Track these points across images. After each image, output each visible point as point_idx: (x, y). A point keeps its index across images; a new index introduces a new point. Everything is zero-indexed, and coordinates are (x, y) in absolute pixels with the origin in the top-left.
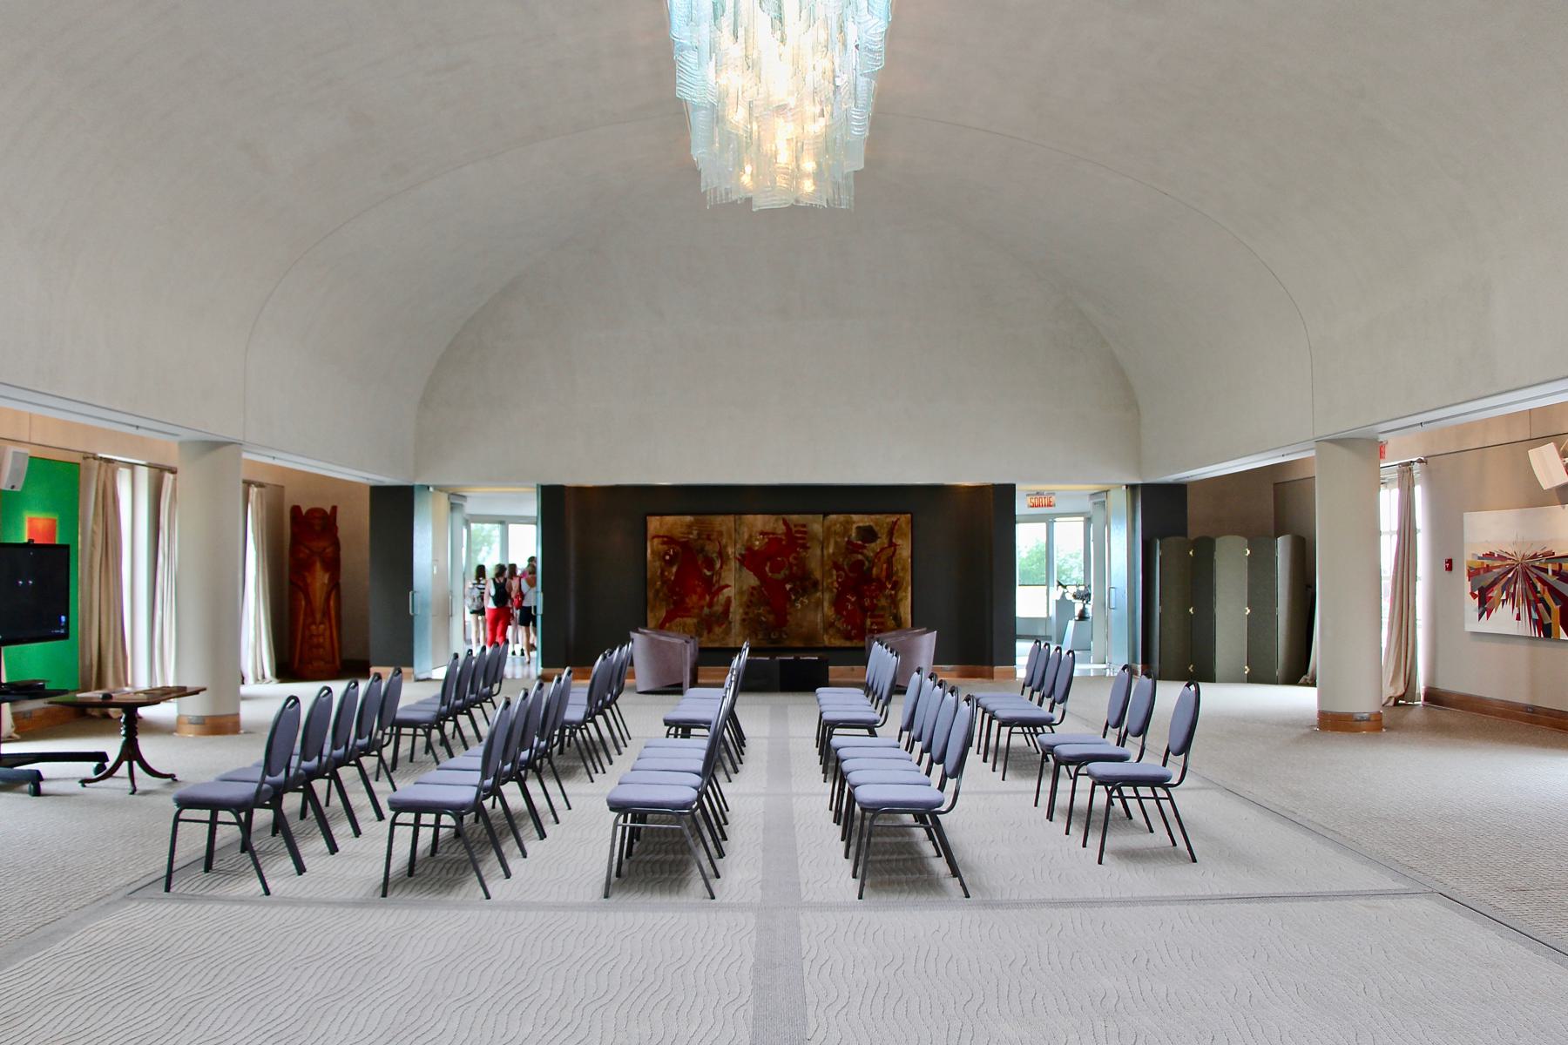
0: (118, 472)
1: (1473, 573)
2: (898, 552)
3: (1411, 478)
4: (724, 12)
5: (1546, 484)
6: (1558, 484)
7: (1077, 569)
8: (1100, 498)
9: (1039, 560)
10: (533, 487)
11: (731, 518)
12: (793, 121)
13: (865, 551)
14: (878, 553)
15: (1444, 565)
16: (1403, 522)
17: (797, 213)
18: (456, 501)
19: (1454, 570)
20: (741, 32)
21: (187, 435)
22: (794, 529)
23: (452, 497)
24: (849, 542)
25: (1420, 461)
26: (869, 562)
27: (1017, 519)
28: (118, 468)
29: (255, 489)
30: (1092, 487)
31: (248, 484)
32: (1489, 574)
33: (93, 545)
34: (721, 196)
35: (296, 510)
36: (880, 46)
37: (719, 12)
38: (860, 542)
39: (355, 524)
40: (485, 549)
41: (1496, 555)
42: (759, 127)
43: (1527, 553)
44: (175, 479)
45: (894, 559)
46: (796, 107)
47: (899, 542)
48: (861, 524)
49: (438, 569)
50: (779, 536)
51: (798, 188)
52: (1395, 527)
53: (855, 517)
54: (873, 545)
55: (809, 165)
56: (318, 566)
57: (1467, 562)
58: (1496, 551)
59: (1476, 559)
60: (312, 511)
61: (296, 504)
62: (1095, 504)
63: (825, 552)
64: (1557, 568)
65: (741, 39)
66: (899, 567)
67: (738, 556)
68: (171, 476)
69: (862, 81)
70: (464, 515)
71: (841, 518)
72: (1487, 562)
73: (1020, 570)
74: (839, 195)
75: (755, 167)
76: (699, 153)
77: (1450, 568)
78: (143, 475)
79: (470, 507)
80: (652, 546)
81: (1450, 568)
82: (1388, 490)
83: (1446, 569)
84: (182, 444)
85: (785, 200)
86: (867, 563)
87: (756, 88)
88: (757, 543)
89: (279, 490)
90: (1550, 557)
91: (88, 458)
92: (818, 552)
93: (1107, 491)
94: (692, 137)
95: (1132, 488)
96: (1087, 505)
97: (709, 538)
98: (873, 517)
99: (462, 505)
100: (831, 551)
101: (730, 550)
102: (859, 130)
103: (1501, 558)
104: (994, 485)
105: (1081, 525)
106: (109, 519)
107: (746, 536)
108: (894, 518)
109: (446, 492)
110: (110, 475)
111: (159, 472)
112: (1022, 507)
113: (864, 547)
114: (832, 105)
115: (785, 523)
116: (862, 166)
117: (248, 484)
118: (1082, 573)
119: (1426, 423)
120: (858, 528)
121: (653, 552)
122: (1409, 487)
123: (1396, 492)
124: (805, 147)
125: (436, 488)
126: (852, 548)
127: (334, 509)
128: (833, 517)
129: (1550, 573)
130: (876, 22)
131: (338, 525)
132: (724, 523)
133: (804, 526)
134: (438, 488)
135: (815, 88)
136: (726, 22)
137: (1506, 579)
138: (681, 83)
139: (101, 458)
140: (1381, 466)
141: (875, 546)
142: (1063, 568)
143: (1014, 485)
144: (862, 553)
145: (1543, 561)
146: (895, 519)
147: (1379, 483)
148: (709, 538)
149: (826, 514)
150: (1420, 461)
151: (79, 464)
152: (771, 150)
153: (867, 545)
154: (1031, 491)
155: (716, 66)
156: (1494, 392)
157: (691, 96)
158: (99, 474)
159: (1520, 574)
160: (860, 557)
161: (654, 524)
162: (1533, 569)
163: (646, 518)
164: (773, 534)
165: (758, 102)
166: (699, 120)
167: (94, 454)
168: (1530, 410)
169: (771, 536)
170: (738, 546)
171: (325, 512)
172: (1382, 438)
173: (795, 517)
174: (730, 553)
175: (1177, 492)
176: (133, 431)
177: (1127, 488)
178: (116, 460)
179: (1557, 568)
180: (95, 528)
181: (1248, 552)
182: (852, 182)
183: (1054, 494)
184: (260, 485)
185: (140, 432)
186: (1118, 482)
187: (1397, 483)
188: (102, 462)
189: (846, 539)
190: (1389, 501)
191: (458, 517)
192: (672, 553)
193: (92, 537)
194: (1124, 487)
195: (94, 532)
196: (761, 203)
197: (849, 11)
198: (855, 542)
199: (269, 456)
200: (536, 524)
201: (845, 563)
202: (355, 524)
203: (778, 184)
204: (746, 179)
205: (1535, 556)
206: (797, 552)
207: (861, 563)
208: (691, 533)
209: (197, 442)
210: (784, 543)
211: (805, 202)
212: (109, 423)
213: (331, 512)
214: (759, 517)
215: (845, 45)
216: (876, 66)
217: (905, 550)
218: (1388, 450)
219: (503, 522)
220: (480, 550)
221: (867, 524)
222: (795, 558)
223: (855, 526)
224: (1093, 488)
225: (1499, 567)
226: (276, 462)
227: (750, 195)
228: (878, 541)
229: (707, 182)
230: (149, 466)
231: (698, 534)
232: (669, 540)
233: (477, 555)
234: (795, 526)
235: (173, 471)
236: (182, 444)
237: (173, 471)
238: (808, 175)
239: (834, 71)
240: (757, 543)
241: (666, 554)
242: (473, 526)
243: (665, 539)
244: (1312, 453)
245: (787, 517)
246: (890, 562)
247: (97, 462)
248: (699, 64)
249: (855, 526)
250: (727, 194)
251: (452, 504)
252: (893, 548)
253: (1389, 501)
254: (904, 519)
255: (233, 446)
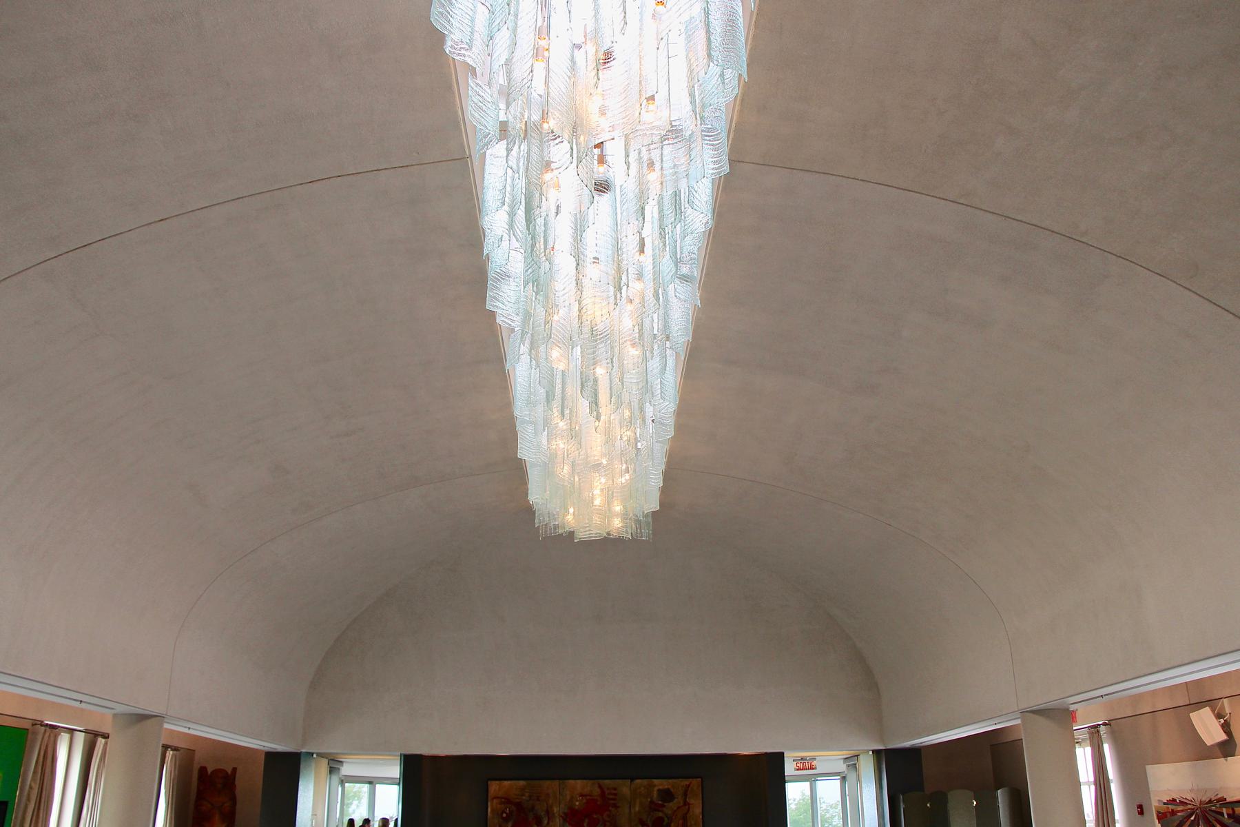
0: (60, 737)
1: (1162, 817)
2: (691, 810)
3: (1100, 737)
4: (554, 397)
5: (1209, 742)
6: (1218, 741)
7: (837, 818)
8: (852, 761)
9: (805, 811)
10: (397, 756)
11: (556, 783)
12: (606, 475)
13: (664, 809)
14: (675, 811)
15: (1136, 810)
16: (1097, 774)
17: (608, 544)
18: (334, 765)
19: (1145, 814)
20: (567, 411)
21: (120, 709)
22: (607, 792)
23: (330, 762)
24: (652, 802)
25: (1105, 724)
26: (668, 818)
27: (786, 778)
28: (60, 734)
29: (171, 752)
30: (844, 753)
31: (166, 747)
32: (1175, 817)
33: (29, 799)
34: (550, 530)
35: (203, 770)
36: (671, 421)
37: (551, 398)
38: (660, 802)
39: (251, 783)
40: (355, 802)
41: (1178, 801)
42: (580, 479)
43: (1203, 799)
44: (106, 743)
45: (688, 816)
46: (608, 465)
47: (692, 801)
48: (661, 787)
49: (316, 822)
50: (596, 798)
51: (609, 524)
52: (1092, 779)
53: (656, 781)
54: (671, 804)
55: (618, 508)
56: (217, 818)
57: (1155, 806)
58: (1177, 796)
59: (1162, 805)
60: (216, 772)
61: (203, 765)
62: (848, 766)
63: (632, 811)
64: (1231, 812)
65: (567, 417)
66: (693, 822)
67: (561, 814)
68: (103, 740)
69: (657, 446)
70: (341, 776)
71: (645, 782)
72: (1171, 807)
73: (790, 819)
74: (641, 531)
75: (576, 509)
76: (534, 496)
77: (1141, 813)
78: (80, 738)
79: (346, 770)
80: (492, 806)
81: (1141, 813)
82: (1082, 749)
83: (1139, 814)
84: (115, 716)
85: (600, 533)
86: (666, 819)
87: (577, 452)
88: (577, 803)
89: (190, 753)
90: (1222, 801)
91: (36, 724)
92: (627, 811)
93: (857, 756)
94: (529, 486)
95: (877, 753)
96: (842, 767)
97: (538, 800)
98: (670, 781)
99: (339, 769)
100: (637, 809)
101: (555, 810)
102: (656, 481)
103: (1182, 803)
104: (766, 753)
105: (838, 782)
106: (46, 775)
107: (568, 797)
108: (686, 782)
109: (327, 758)
110: (52, 739)
111: (93, 737)
112: (790, 768)
113: (664, 806)
114: (635, 464)
115: (600, 787)
116: (658, 508)
117: (166, 747)
118: (841, 820)
119: (1105, 695)
120: (659, 790)
121: (492, 810)
122: (1099, 745)
123: (1089, 750)
124: (615, 495)
125: (318, 754)
126: (654, 807)
127: (234, 770)
128: (638, 781)
129: (1226, 816)
130: (667, 404)
131: (236, 783)
132: (550, 786)
133: (615, 789)
134: (321, 755)
135: (622, 451)
136: (556, 404)
137: (1188, 823)
138: (521, 448)
139: (47, 724)
140: (1074, 728)
141: (673, 805)
142: (826, 817)
143: (783, 753)
144: (662, 811)
145: (1218, 806)
146: (688, 783)
147: (1073, 743)
148: (538, 800)
149: (632, 779)
150: (1105, 724)
151: (28, 730)
152: (589, 496)
153: (666, 804)
154: (796, 757)
155: (548, 436)
156: (1155, 670)
157: (529, 457)
158: (43, 738)
159: (1201, 817)
160: (660, 814)
161: (494, 787)
162: (1211, 813)
163: (487, 782)
164: (590, 796)
165: (579, 462)
166: (534, 475)
167: (42, 722)
168: (1186, 683)
169: (588, 797)
170: (562, 806)
171: (227, 773)
172: (1072, 708)
173: (607, 782)
174: (555, 811)
175: (915, 753)
176: (77, 704)
177: (873, 753)
178: (59, 727)
179: (1231, 812)
180: (33, 784)
181: (975, 803)
182: (650, 519)
183: (815, 759)
184: (175, 749)
185: (83, 705)
186: (866, 748)
187: (1088, 742)
188: (47, 728)
189: (649, 800)
190: (1084, 756)
191: (335, 779)
192: (508, 812)
193: (29, 791)
194: (871, 753)
195: (31, 787)
196: (581, 535)
197: (647, 397)
198: (657, 802)
199: (185, 727)
200: (399, 784)
201: (649, 820)
202: (251, 783)
203: (594, 522)
204: (570, 518)
205: (1210, 801)
206: (610, 811)
207: (661, 819)
208: (523, 795)
209: (125, 714)
210: (599, 803)
211: (615, 534)
212: (56, 697)
213: (232, 772)
214: (579, 781)
215: (644, 420)
216: (668, 435)
217: (697, 810)
218: (1078, 715)
219: (371, 782)
220: (351, 804)
221: (666, 787)
222: (609, 816)
223: (656, 789)
224: (846, 754)
225: (1182, 811)
226: (191, 732)
227: (572, 529)
228: (676, 800)
229: (540, 520)
230: (86, 732)
231: (530, 796)
232: (507, 801)
233: (349, 807)
234: (608, 789)
235: (106, 736)
236: (115, 716)
237: (106, 736)
238: (617, 516)
239: (636, 439)
240: (577, 803)
241: (503, 812)
242: (347, 785)
243: (503, 800)
244: (1018, 722)
245: (601, 781)
246: (685, 818)
247: (43, 728)
248: (536, 434)
249: (656, 789)
250: (555, 529)
251: (330, 767)
252: (687, 807)
253: (1084, 756)
254: (696, 782)
255: (153, 719)
